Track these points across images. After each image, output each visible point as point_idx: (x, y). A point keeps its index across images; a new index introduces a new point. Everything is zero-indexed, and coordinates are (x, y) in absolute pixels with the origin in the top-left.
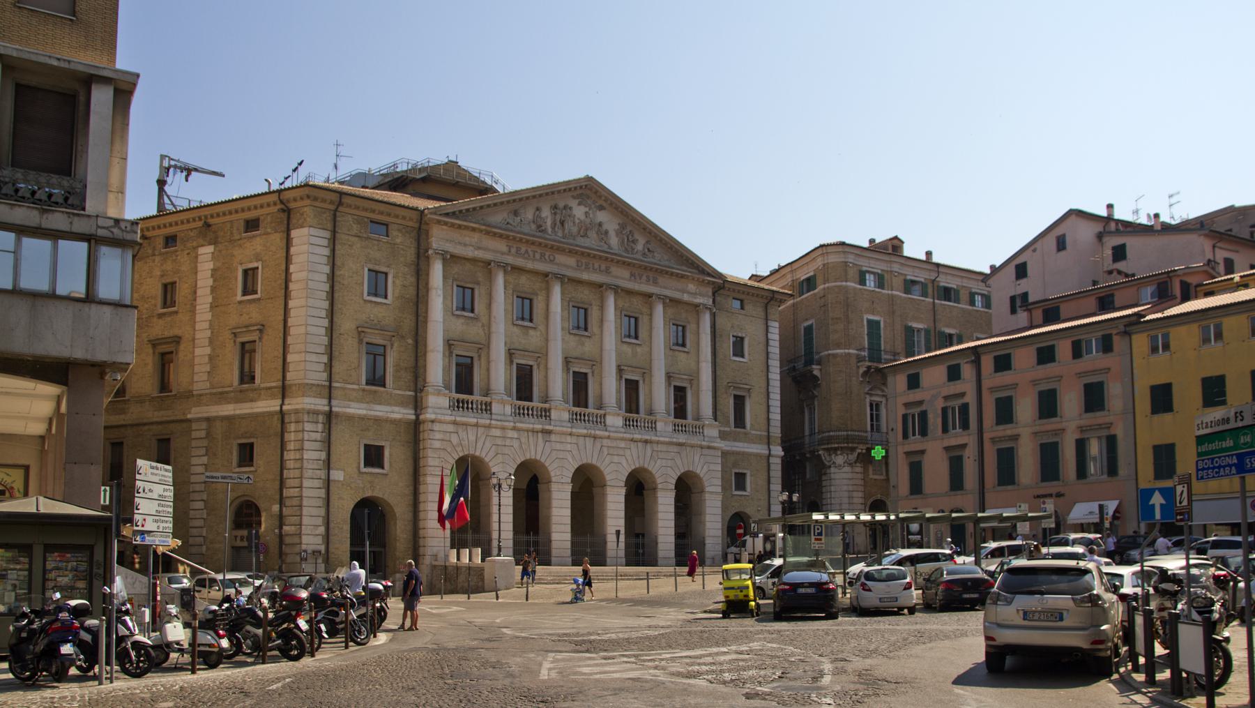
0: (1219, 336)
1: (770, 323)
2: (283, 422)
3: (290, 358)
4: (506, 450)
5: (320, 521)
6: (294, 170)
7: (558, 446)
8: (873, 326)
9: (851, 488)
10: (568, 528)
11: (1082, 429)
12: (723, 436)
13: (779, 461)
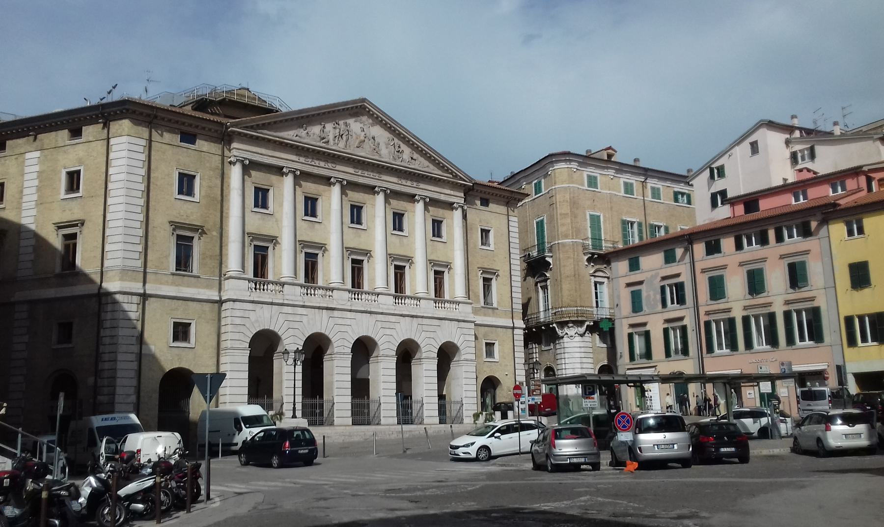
0: (861, 231)
1: (511, 218)
2: (100, 304)
3: (107, 248)
4: (296, 325)
5: (132, 391)
6: (109, 93)
7: (340, 321)
8: (595, 221)
9: (583, 355)
10: (349, 392)
11: (745, 308)
12: (476, 311)
13: (521, 332)
